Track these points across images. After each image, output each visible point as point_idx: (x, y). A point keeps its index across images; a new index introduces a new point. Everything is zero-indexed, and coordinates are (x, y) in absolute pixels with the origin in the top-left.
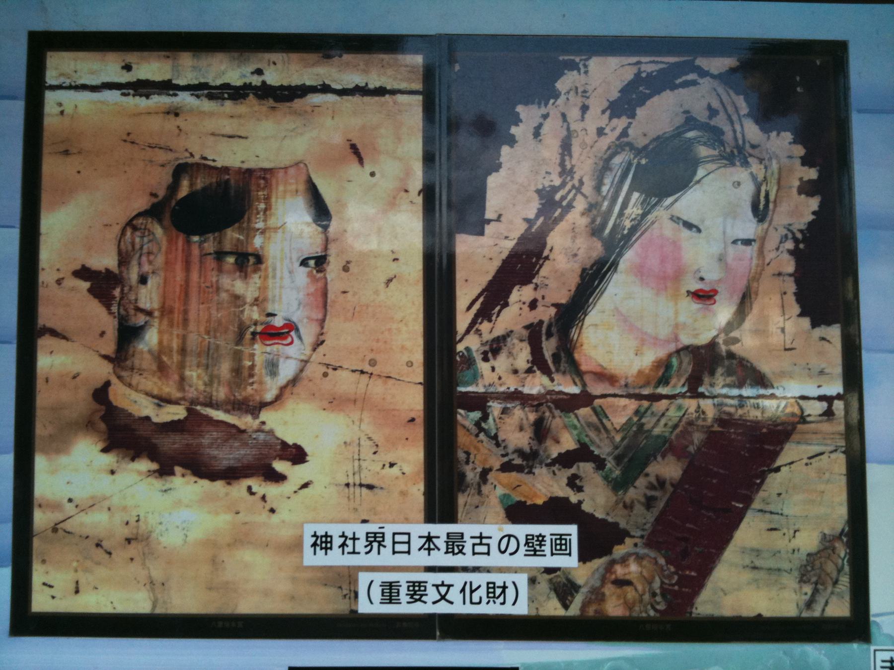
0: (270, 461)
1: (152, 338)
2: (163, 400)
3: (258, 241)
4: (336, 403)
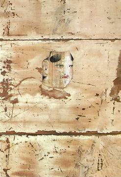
0: (65, 96)
1: (47, 78)
2: (50, 87)
3: (63, 63)
4: (75, 87)
